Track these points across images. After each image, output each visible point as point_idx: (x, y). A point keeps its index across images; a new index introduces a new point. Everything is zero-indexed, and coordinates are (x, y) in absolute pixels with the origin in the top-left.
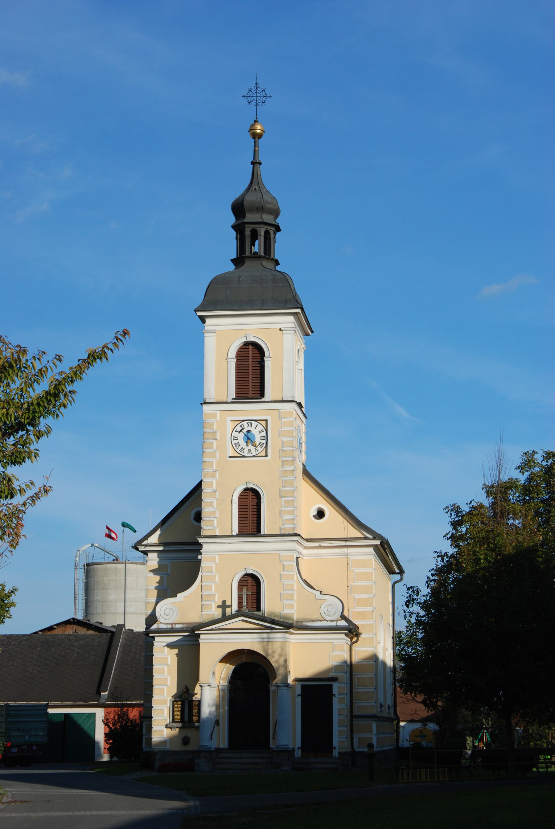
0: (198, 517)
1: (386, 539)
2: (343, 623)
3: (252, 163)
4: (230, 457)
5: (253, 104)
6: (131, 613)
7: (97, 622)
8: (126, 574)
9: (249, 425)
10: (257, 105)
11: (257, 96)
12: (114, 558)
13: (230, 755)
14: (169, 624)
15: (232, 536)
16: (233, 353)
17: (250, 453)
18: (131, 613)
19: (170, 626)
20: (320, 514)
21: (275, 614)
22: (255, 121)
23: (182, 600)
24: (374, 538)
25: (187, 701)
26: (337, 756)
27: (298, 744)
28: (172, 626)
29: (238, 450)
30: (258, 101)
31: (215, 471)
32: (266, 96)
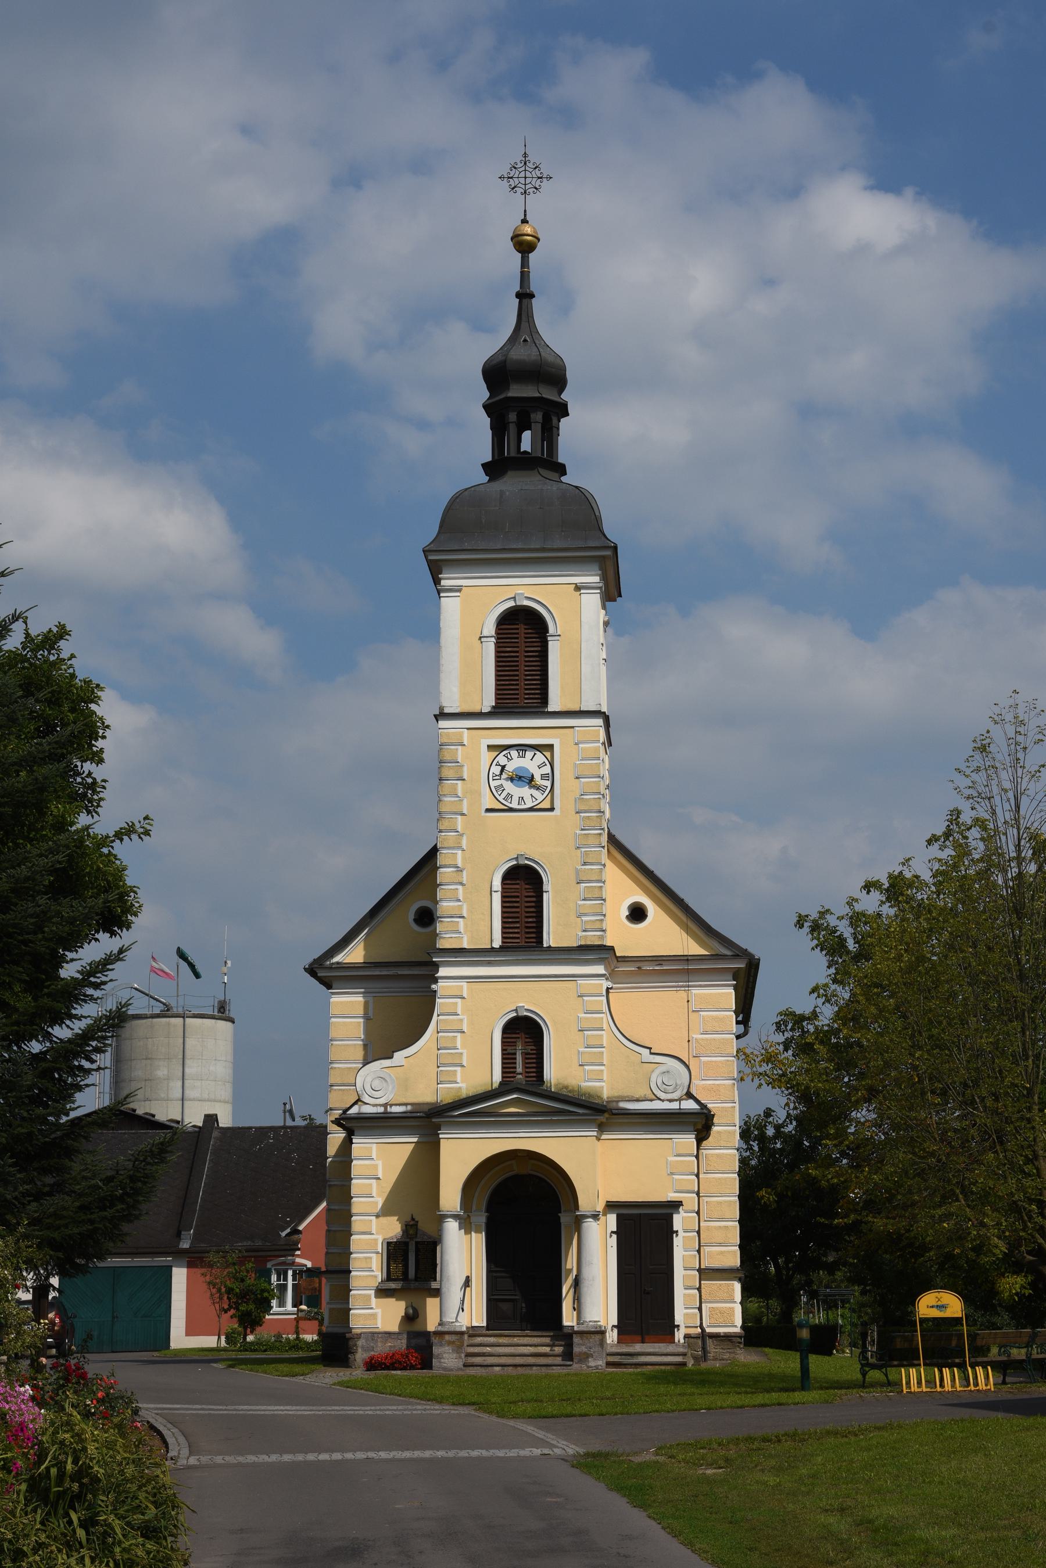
0: (427, 917)
1: (756, 957)
2: (690, 1105)
3: (518, 295)
4: (488, 810)
5: (519, 190)
6: (194, 1100)
7: (146, 1114)
8: (186, 1035)
9: (521, 754)
10: (525, 192)
11: (525, 178)
12: (162, 1007)
13: (492, 1340)
14: (380, 1105)
15: (492, 950)
16: (490, 629)
17: (523, 803)
18: (194, 1100)
19: (381, 1110)
20: (637, 914)
21: (570, 1088)
22: (522, 220)
23: (403, 1062)
24: (736, 956)
25: (414, 1243)
26: (682, 1341)
27: (614, 1320)
28: (386, 1108)
29: (500, 798)
30: (528, 187)
31: (462, 835)
32: (541, 178)
